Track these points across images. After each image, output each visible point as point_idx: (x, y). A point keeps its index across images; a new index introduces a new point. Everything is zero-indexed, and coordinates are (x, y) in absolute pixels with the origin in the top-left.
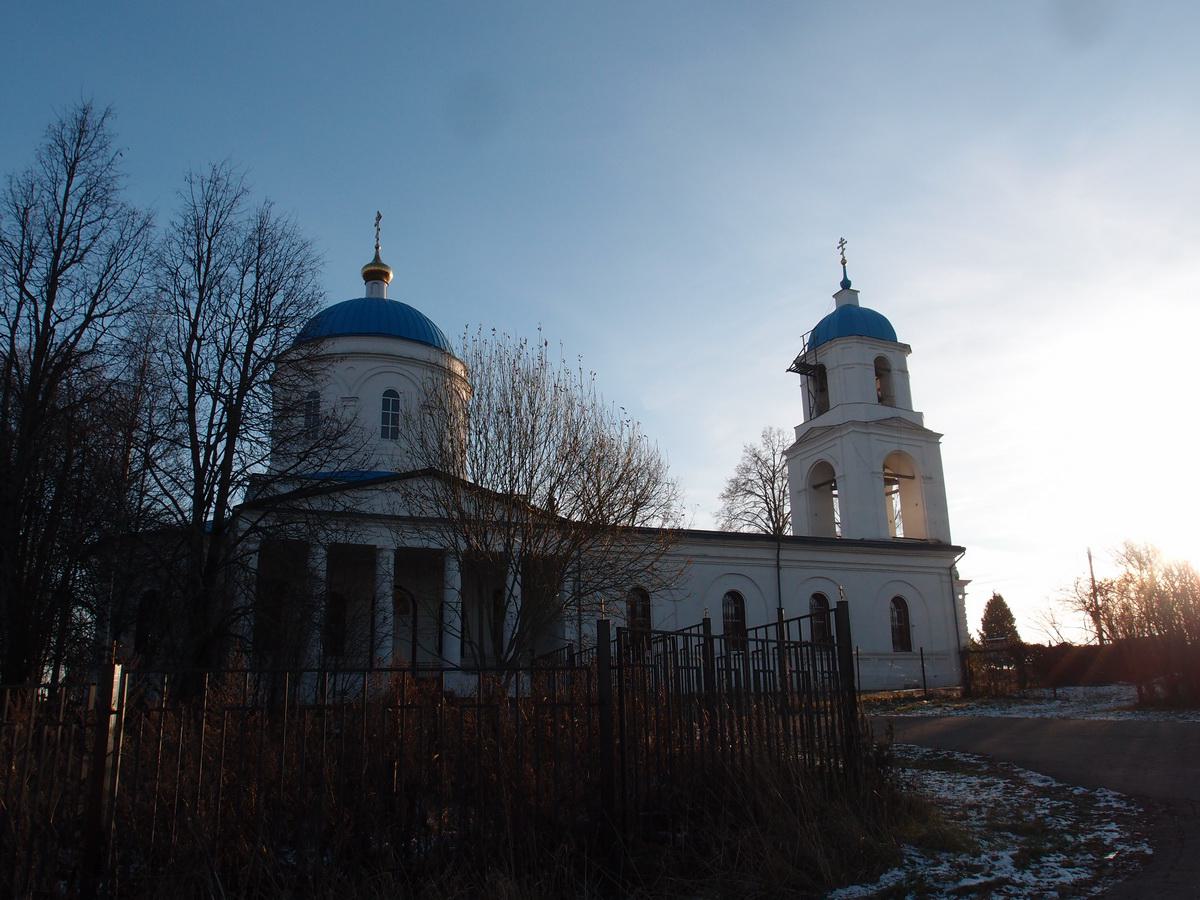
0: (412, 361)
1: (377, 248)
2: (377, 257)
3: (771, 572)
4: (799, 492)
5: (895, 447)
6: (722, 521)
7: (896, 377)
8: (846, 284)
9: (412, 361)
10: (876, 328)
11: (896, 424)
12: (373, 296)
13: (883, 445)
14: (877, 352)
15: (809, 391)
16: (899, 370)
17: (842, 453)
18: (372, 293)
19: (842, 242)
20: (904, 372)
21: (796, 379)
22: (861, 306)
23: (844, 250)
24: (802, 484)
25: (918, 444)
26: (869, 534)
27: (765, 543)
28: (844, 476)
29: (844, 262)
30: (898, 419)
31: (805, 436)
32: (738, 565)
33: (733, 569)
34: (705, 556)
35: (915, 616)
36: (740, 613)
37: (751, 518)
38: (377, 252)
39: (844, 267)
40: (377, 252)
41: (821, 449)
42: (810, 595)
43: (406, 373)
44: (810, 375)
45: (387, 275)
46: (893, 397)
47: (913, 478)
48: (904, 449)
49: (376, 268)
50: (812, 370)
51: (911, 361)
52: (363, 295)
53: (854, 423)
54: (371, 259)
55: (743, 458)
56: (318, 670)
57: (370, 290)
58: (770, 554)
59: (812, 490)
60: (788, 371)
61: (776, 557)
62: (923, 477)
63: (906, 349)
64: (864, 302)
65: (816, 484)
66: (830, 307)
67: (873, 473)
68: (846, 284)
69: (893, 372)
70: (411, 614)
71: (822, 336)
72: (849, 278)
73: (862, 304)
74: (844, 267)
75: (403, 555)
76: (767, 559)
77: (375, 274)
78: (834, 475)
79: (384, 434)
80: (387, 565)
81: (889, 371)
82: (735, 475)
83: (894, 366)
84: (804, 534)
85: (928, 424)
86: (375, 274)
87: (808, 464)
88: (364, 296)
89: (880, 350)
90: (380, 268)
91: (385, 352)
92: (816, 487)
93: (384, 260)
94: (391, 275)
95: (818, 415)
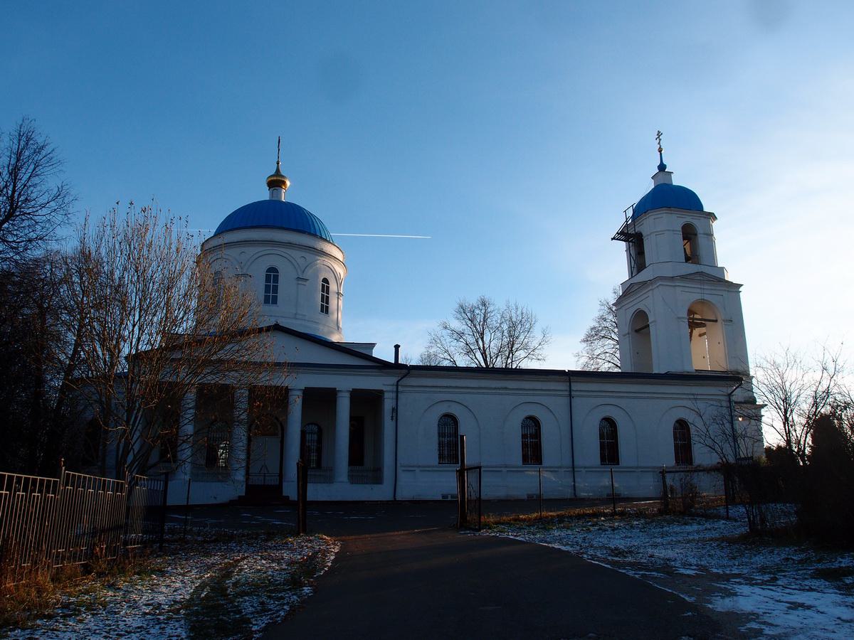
0: (290, 245)
1: (278, 163)
2: (278, 170)
4: (624, 336)
5: (698, 297)
6: (584, 360)
7: (701, 240)
8: (662, 167)
9: (290, 245)
11: (699, 278)
12: (273, 199)
13: (687, 296)
14: (685, 220)
15: (630, 254)
16: (705, 234)
19: (659, 134)
20: (710, 235)
21: (622, 245)
22: (674, 184)
23: (660, 140)
24: (626, 330)
25: (720, 293)
26: (676, 368)
28: (654, 321)
29: (660, 150)
30: (701, 274)
31: (629, 291)
32: (533, 395)
34: (506, 388)
35: (467, 429)
36: (537, 435)
37: (607, 357)
38: (278, 167)
39: (661, 154)
40: (278, 167)
42: (676, 419)
43: (282, 254)
44: (631, 241)
45: (284, 183)
47: (716, 321)
48: (706, 297)
50: (632, 237)
51: (716, 226)
54: (273, 172)
55: (600, 310)
57: (272, 194)
58: (563, 386)
60: (612, 239)
62: (724, 321)
63: (712, 216)
64: (677, 181)
65: (637, 328)
66: (650, 186)
67: (679, 318)
68: (662, 167)
69: (699, 235)
70: (280, 436)
71: (643, 208)
72: (665, 163)
73: (675, 183)
74: (661, 154)
75: (309, 394)
77: (276, 183)
78: (648, 321)
79: (267, 301)
81: (696, 235)
83: (700, 230)
84: (629, 369)
85: (730, 277)
86: (276, 183)
88: (268, 199)
89: (688, 218)
92: (637, 331)
93: (282, 173)
94: (288, 183)
95: (639, 271)
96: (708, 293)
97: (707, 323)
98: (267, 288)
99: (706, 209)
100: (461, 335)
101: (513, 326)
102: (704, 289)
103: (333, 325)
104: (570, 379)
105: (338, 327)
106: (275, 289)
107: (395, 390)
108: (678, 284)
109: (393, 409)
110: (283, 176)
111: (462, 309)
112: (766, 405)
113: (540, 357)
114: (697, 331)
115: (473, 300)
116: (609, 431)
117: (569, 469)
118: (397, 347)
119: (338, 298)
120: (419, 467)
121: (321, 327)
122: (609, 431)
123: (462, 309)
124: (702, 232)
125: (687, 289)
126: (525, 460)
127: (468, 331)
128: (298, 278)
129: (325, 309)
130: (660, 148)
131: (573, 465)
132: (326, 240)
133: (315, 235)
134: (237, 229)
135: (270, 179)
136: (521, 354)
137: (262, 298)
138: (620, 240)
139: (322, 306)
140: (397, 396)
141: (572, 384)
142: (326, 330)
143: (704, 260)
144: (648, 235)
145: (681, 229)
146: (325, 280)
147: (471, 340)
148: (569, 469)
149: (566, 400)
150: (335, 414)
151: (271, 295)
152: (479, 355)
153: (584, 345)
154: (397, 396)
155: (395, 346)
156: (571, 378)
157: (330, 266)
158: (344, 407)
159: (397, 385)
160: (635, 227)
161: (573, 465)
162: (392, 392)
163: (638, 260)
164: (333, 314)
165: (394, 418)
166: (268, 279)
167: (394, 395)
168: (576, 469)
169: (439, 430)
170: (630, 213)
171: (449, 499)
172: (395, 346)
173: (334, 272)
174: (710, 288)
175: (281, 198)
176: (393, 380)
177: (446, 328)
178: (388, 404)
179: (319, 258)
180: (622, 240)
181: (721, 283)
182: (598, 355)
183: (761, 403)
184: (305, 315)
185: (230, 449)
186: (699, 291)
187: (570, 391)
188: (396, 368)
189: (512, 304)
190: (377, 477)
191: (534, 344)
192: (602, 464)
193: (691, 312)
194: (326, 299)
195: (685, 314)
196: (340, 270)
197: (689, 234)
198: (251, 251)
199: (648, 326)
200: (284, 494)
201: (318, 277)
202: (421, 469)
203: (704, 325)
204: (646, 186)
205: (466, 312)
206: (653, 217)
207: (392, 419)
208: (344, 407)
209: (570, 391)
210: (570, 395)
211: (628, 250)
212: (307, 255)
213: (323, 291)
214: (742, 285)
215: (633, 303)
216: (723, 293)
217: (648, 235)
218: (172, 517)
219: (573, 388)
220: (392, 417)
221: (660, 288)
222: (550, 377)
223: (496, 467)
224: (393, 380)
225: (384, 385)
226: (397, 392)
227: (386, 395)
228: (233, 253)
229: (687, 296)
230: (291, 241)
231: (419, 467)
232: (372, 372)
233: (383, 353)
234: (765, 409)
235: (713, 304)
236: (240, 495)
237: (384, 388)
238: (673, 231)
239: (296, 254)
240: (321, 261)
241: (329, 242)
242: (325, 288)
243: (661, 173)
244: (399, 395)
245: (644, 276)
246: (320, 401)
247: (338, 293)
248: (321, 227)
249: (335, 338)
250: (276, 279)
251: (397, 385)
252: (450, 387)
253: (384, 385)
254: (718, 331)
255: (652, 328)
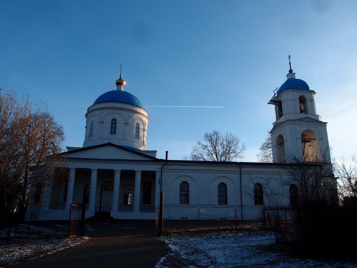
0: (122, 109)
1: (121, 75)
2: (120, 78)
3: (238, 176)
4: (274, 146)
5: (306, 128)
6: (261, 157)
7: (308, 103)
8: (291, 71)
9: (122, 109)
10: (302, 86)
11: (306, 120)
13: (302, 128)
16: (309, 100)
17: (286, 132)
18: (118, 89)
19: (289, 56)
20: (312, 101)
21: (273, 106)
23: (290, 59)
24: (275, 144)
25: (316, 126)
27: (234, 165)
28: (286, 140)
31: (276, 126)
32: (224, 173)
33: (222, 175)
34: (211, 170)
39: (290, 65)
41: (281, 130)
43: (95, 115)
44: (277, 104)
46: (307, 110)
47: (315, 139)
48: (310, 129)
49: (120, 81)
50: (276, 102)
51: (315, 97)
52: (116, 89)
53: (289, 120)
54: (118, 79)
56: (272, 210)
57: (118, 88)
58: (237, 169)
59: (278, 145)
60: (268, 104)
61: (239, 170)
62: (318, 139)
63: (313, 92)
64: (297, 77)
67: (297, 138)
68: (291, 71)
69: (307, 101)
71: (281, 90)
72: (292, 69)
73: (297, 78)
74: (290, 65)
75: (100, 172)
76: (237, 171)
79: (111, 133)
80: (72, 175)
81: (306, 101)
82: (265, 142)
84: (276, 162)
86: (119, 83)
87: (277, 136)
90: (121, 81)
91: (113, 107)
92: (279, 144)
93: (122, 78)
94: (125, 83)
95: (280, 118)
96: (311, 127)
97: (312, 140)
98: (112, 128)
99: (311, 89)
100: (206, 147)
101: (229, 143)
102: (309, 125)
103: (141, 143)
104: (240, 166)
105: (144, 144)
106: (115, 128)
107: (161, 171)
108: (296, 123)
109: (160, 179)
110: (123, 80)
111: (206, 135)
112: (339, 178)
113: (241, 156)
114: (307, 144)
115: (210, 132)
116: (185, 187)
117: (239, 207)
118: (167, 152)
119: (144, 132)
120: (171, 205)
121: (135, 144)
122: (185, 187)
123: (206, 135)
124: (308, 99)
125: (300, 125)
126: (256, 202)
127: (209, 144)
128: (125, 123)
129: (138, 136)
130: (290, 62)
131: (242, 205)
132: (139, 107)
133: (133, 105)
134: (98, 103)
135: (117, 82)
136: (232, 155)
137: (110, 131)
138: (271, 104)
139: (136, 135)
140: (162, 174)
141: (241, 168)
142: (137, 145)
143: (309, 111)
144: (283, 102)
145: (298, 98)
146: (138, 124)
147: (210, 148)
148: (239, 207)
149: (239, 175)
150: (114, 179)
151: (113, 131)
152: (214, 156)
153: (261, 151)
154: (162, 174)
155: (166, 152)
156: (241, 165)
157: (140, 118)
158: (138, 178)
159: (162, 169)
160: (278, 98)
161: (242, 205)
162: (159, 172)
163: (280, 113)
164: (141, 138)
165: (160, 183)
166: (112, 123)
167: (160, 173)
168: (243, 207)
169: (180, 189)
170: (276, 92)
171: (184, 219)
172: (166, 152)
173: (142, 120)
174: (307, 124)
175: (121, 89)
176: (160, 167)
177: (199, 144)
178: (158, 177)
179: (135, 114)
180: (273, 104)
181: (317, 122)
182: (268, 155)
183: (337, 177)
184: (128, 139)
185: (133, 197)
186: (307, 126)
187: (241, 171)
188: (166, 162)
189: (229, 133)
190: (152, 210)
191: (238, 150)
192: (219, 204)
193: (303, 135)
194: (138, 132)
195: (299, 136)
196: (146, 120)
197: (302, 100)
198: (106, 112)
199: (283, 142)
200: (111, 216)
201: (134, 123)
202: (171, 206)
203: (310, 141)
204: (282, 80)
205: (209, 138)
206: (285, 93)
207: (159, 184)
208: (138, 178)
209: (241, 171)
210: (241, 173)
211: (276, 108)
212: (129, 113)
213: (136, 128)
214: (327, 123)
215: (277, 132)
216: (318, 127)
217: (283, 102)
218: (57, 226)
219: (242, 170)
220: (159, 183)
221: (288, 125)
222: (231, 165)
223: (206, 205)
224: (160, 167)
225: (156, 169)
226: (162, 172)
227: (157, 173)
228: (98, 113)
229: (302, 128)
230: (123, 107)
231: (171, 205)
232: (145, 163)
233: (160, 156)
234: (339, 179)
235: (314, 132)
236: (92, 216)
237: (156, 170)
238: (295, 99)
239: (124, 113)
240: (136, 115)
241: (140, 108)
242: (138, 128)
243: (290, 74)
244: (163, 173)
245: (282, 119)
246: (128, 176)
247: (144, 129)
248: (136, 101)
249: (142, 148)
250: (116, 124)
251: (162, 169)
252: (179, 169)
253: (156, 169)
254: (315, 143)
255: (285, 143)
